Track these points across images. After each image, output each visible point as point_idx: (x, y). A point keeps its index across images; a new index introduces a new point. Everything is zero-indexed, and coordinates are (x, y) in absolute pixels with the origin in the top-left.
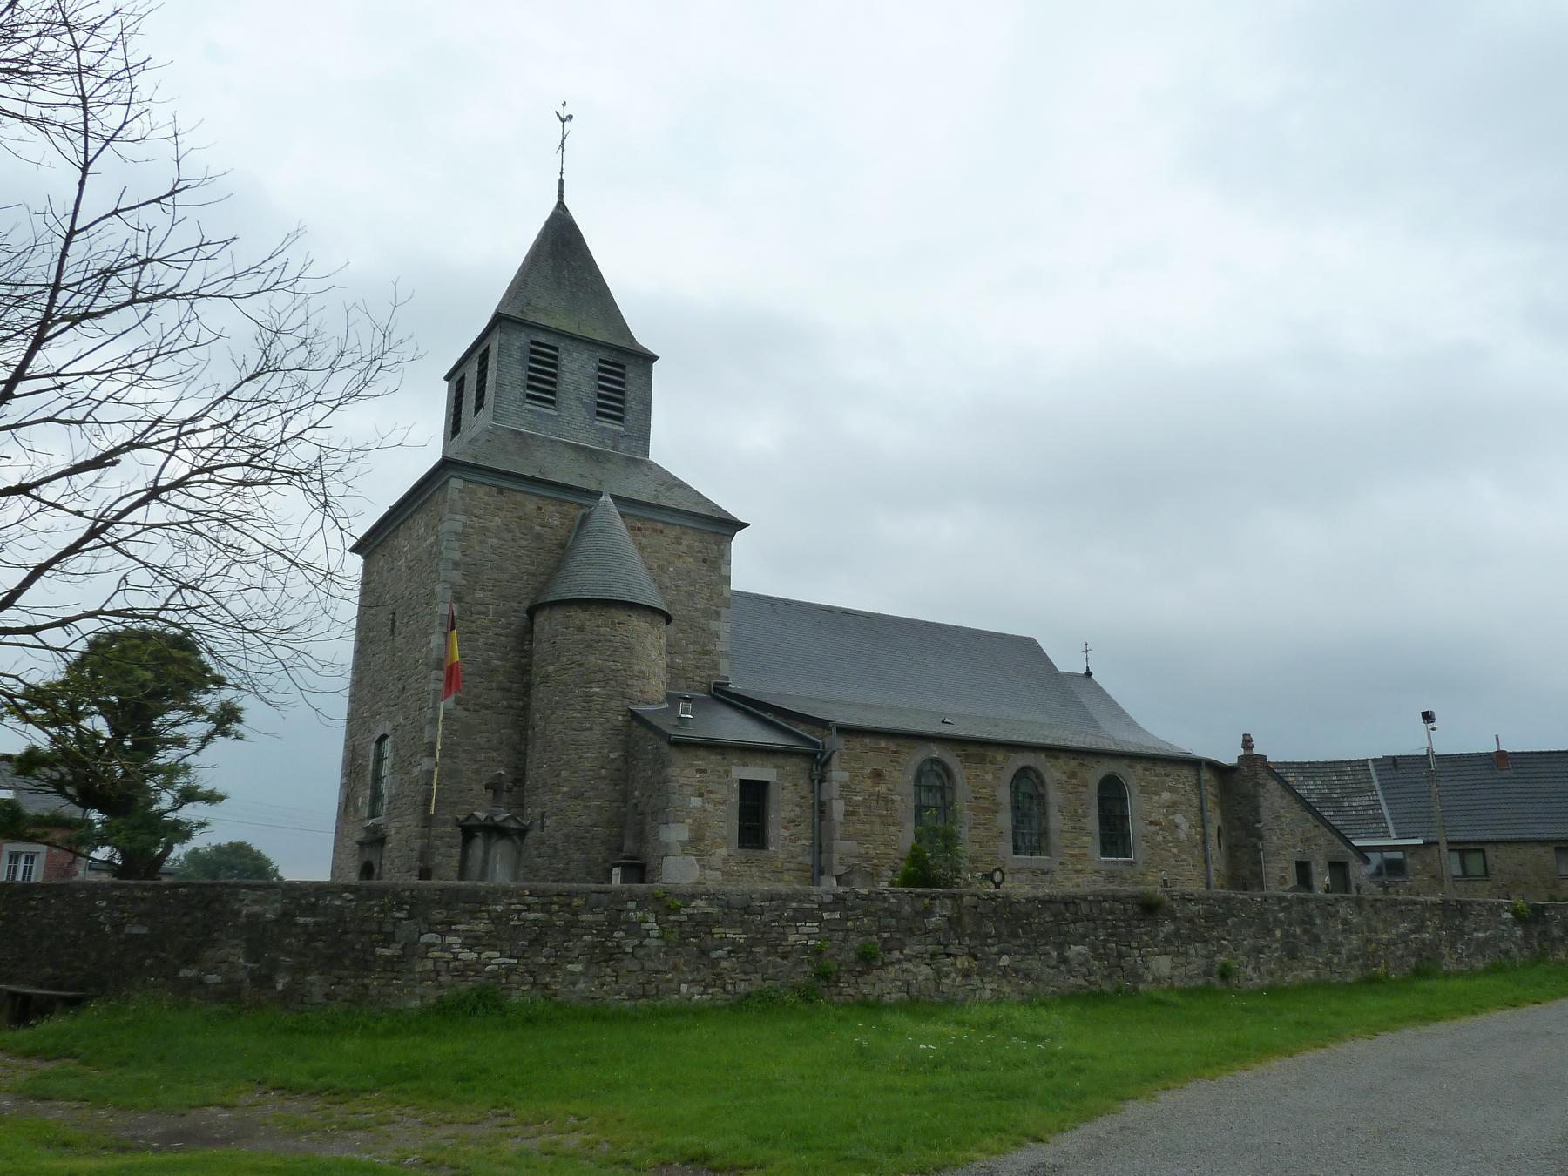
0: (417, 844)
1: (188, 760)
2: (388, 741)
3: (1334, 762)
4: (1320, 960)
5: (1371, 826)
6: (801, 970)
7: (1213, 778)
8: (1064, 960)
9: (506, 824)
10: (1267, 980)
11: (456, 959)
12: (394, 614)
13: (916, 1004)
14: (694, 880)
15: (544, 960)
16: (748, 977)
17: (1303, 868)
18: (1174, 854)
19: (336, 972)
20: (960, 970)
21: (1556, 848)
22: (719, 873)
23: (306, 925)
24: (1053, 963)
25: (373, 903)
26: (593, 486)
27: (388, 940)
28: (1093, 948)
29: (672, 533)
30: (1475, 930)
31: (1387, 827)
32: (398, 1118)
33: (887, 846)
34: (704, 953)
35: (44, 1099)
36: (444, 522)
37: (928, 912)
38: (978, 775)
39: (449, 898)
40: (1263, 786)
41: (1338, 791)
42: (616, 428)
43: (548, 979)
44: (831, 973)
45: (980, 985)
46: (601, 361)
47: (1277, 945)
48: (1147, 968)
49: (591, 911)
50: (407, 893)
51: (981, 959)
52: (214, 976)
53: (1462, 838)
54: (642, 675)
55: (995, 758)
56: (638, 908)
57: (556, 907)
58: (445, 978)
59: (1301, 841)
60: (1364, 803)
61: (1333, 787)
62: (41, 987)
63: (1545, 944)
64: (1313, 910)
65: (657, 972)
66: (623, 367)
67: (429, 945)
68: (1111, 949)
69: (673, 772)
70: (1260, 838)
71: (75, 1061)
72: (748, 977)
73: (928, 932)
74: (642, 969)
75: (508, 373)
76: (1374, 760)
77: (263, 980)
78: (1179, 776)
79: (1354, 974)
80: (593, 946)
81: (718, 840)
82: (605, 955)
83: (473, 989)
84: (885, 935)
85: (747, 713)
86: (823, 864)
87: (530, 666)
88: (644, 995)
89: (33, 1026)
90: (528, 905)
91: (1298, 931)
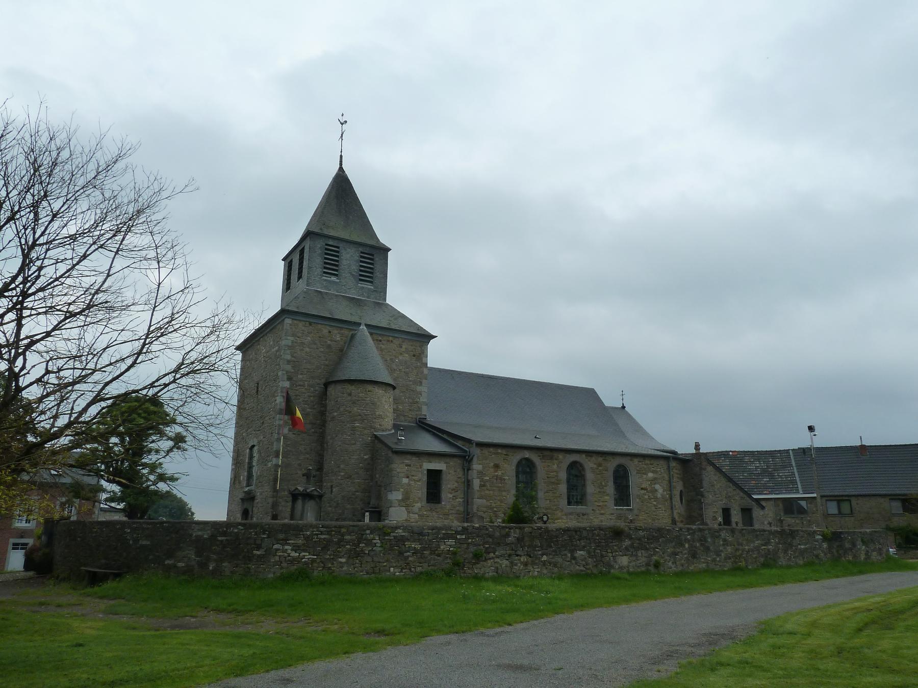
0: (270, 500)
1: (161, 461)
2: (256, 448)
3: (771, 451)
4: (709, 559)
5: (789, 486)
6: (446, 562)
7: (678, 465)
8: (574, 558)
9: (313, 493)
10: (680, 568)
11: (289, 556)
12: (258, 384)
13: (499, 577)
14: (404, 519)
15: (328, 556)
16: (421, 565)
17: (726, 512)
18: (654, 505)
19: (236, 562)
20: (522, 562)
21: (890, 499)
22: (417, 515)
23: (222, 541)
24: (569, 559)
25: (252, 531)
26: (357, 320)
27: (258, 547)
28: (589, 552)
29: (396, 342)
30: (799, 544)
31: (798, 487)
32: (265, 621)
33: (501, 501)
34: (401, 553)
35: (116, 614)
36: (282, 340)
37: (508, 535)
38: (549, 466)
39: (286, 528)
40: (705, 469)
41: (772, 467)
42: (369, 287)
43: (330, 565)
44: (460, 563)
45: (532, 569)
46: (362, 252)
47: (686, 551)
48: (615, 562)
49: (349, 534)
50: (267, 526)
51: (532, 557)
52: (181, 563)
53: (838, 494)
54: (380, 417)
55: (558, 457)
56: (371, 533)
57: (334, 533)
58: (284, 565)
59: (726, 497)
60: (786, 474)
61: (769, 465)
62: (100, 568)
63: (841, 552)
64: (707, 534)
65: (380, 562)
66: (373, 255)
67: (277, 550)
68: (598, 553)
69: (394, 466)
70: (703, 496)
71: (123, 600)
72: (421, 565)
73: (507, 544)
74: (373, 561)
75: (314, 261)
76: (793, 450)
77: (203, 565)
78: (658, 465)
79: (728, 565)
80: (350, 550)
81: (417, 499)
82: (356, 554)
83: (296, 569)
84: (487, 546)
85: (434, 435)
86: (469, 511)
87: (326, 411)
88: (374, 573)
89: (101, 585)
90: (321, 532)
91: (698, 544)
